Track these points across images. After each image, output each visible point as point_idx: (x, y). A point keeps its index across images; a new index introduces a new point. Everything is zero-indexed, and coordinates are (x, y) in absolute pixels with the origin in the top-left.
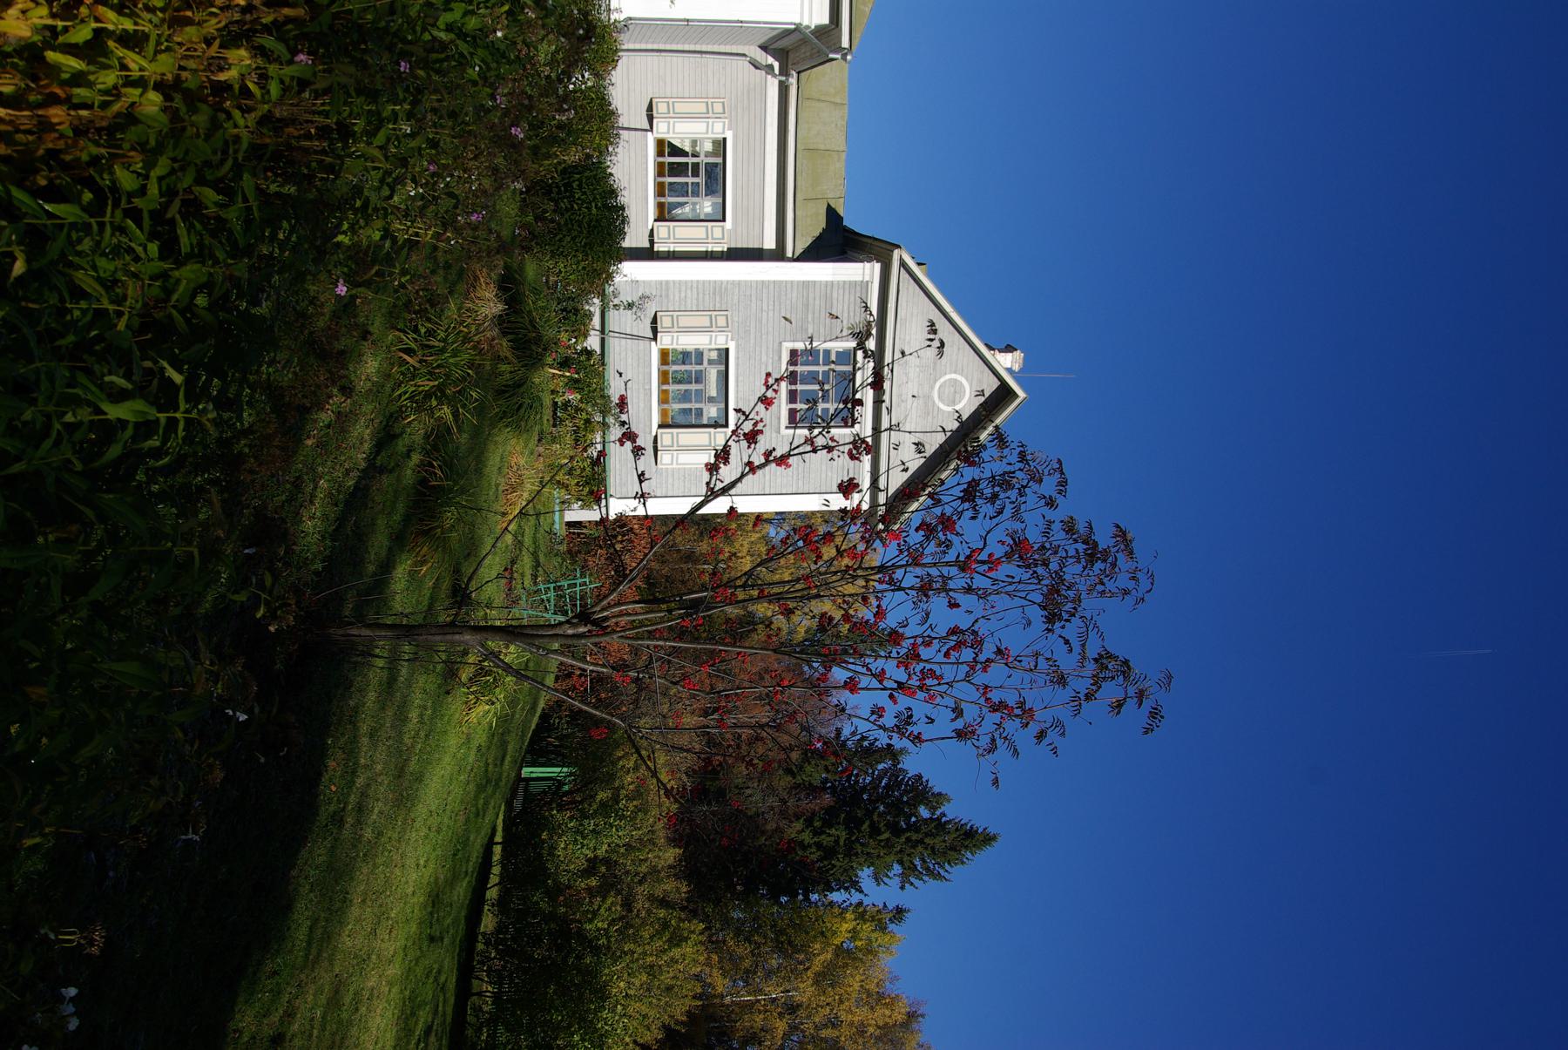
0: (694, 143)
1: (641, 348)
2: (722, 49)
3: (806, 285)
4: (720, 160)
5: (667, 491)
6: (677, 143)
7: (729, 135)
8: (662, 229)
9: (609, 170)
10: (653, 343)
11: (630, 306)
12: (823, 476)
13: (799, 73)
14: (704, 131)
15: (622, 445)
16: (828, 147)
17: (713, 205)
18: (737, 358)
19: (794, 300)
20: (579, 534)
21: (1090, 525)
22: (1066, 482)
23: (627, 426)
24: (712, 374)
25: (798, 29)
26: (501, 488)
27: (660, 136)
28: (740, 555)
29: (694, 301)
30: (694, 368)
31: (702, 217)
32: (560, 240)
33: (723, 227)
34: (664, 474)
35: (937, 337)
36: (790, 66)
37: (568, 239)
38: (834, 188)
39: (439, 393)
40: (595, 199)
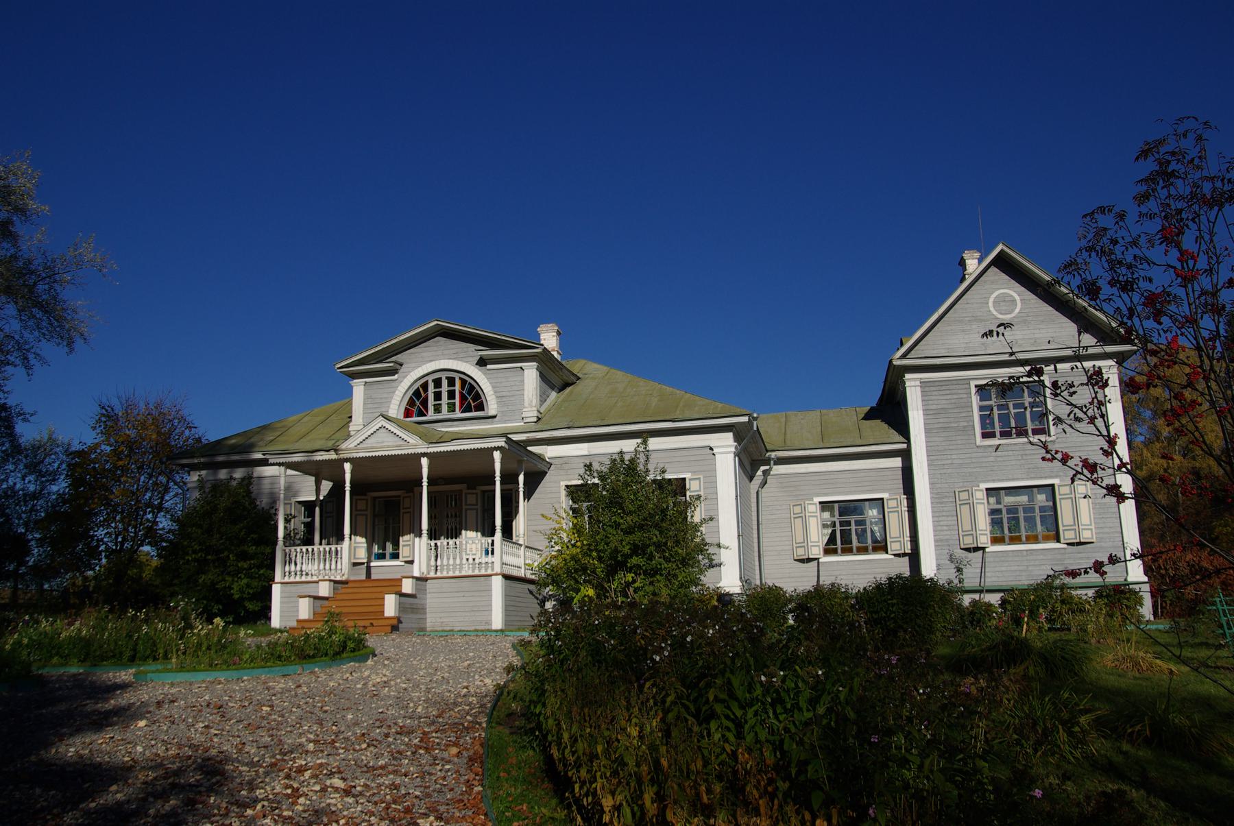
0: (824, 526)
1: (992, 559)
2: (754, 509)
3: (928, 431)
4: (836, 506)
5: (1116, 532)
6: (826, 539)
7: (817, 500)
8: (894, 547)
9: (862, 591)
10: (987, 550)
11: (959, 570)
13: (767, 451)
14: (815, 519)
15: (1106, 573)
16: (819, 424)
17: (871, 508)
18: (994, 481)
19: (941, 439)
20: (1162, 607)
21: (1139, 182)
22: (1101, 207)
23: (1089, 570)
24: (1009, 500)
25: (737, 454)
26: (1137, 675)
27: (822, 552)
28: (1165, 466)
29: (950, 518)
30: (1005, 516)
31: (881, 516)
32: (919, 626)
33: (1059, 486)
34: (1101, 535)
35: (995, 329)
36: (763, 458)
37: (918, 621)
38: (849, 416)
39: (1069, 724)
40: (885, 601)
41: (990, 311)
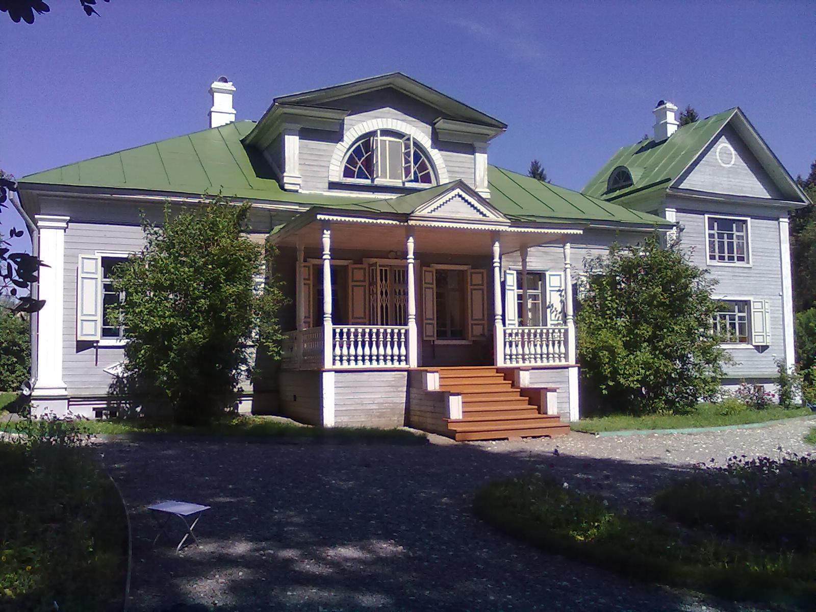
12: (771, 240)
41: (717, 159)
